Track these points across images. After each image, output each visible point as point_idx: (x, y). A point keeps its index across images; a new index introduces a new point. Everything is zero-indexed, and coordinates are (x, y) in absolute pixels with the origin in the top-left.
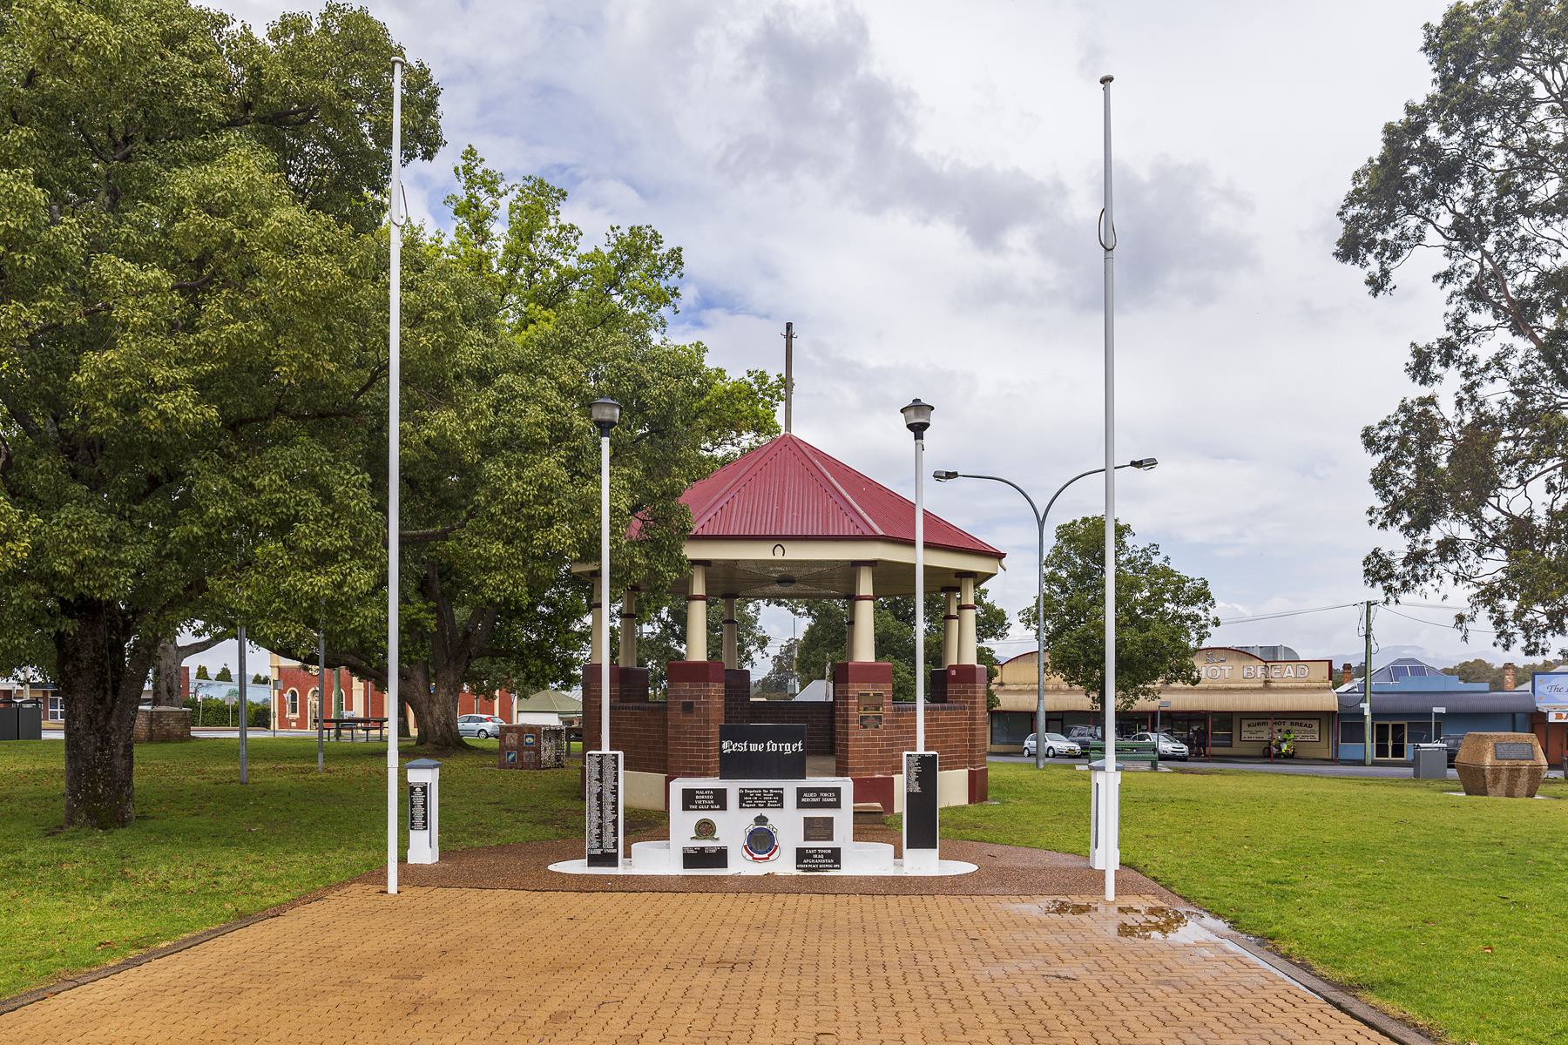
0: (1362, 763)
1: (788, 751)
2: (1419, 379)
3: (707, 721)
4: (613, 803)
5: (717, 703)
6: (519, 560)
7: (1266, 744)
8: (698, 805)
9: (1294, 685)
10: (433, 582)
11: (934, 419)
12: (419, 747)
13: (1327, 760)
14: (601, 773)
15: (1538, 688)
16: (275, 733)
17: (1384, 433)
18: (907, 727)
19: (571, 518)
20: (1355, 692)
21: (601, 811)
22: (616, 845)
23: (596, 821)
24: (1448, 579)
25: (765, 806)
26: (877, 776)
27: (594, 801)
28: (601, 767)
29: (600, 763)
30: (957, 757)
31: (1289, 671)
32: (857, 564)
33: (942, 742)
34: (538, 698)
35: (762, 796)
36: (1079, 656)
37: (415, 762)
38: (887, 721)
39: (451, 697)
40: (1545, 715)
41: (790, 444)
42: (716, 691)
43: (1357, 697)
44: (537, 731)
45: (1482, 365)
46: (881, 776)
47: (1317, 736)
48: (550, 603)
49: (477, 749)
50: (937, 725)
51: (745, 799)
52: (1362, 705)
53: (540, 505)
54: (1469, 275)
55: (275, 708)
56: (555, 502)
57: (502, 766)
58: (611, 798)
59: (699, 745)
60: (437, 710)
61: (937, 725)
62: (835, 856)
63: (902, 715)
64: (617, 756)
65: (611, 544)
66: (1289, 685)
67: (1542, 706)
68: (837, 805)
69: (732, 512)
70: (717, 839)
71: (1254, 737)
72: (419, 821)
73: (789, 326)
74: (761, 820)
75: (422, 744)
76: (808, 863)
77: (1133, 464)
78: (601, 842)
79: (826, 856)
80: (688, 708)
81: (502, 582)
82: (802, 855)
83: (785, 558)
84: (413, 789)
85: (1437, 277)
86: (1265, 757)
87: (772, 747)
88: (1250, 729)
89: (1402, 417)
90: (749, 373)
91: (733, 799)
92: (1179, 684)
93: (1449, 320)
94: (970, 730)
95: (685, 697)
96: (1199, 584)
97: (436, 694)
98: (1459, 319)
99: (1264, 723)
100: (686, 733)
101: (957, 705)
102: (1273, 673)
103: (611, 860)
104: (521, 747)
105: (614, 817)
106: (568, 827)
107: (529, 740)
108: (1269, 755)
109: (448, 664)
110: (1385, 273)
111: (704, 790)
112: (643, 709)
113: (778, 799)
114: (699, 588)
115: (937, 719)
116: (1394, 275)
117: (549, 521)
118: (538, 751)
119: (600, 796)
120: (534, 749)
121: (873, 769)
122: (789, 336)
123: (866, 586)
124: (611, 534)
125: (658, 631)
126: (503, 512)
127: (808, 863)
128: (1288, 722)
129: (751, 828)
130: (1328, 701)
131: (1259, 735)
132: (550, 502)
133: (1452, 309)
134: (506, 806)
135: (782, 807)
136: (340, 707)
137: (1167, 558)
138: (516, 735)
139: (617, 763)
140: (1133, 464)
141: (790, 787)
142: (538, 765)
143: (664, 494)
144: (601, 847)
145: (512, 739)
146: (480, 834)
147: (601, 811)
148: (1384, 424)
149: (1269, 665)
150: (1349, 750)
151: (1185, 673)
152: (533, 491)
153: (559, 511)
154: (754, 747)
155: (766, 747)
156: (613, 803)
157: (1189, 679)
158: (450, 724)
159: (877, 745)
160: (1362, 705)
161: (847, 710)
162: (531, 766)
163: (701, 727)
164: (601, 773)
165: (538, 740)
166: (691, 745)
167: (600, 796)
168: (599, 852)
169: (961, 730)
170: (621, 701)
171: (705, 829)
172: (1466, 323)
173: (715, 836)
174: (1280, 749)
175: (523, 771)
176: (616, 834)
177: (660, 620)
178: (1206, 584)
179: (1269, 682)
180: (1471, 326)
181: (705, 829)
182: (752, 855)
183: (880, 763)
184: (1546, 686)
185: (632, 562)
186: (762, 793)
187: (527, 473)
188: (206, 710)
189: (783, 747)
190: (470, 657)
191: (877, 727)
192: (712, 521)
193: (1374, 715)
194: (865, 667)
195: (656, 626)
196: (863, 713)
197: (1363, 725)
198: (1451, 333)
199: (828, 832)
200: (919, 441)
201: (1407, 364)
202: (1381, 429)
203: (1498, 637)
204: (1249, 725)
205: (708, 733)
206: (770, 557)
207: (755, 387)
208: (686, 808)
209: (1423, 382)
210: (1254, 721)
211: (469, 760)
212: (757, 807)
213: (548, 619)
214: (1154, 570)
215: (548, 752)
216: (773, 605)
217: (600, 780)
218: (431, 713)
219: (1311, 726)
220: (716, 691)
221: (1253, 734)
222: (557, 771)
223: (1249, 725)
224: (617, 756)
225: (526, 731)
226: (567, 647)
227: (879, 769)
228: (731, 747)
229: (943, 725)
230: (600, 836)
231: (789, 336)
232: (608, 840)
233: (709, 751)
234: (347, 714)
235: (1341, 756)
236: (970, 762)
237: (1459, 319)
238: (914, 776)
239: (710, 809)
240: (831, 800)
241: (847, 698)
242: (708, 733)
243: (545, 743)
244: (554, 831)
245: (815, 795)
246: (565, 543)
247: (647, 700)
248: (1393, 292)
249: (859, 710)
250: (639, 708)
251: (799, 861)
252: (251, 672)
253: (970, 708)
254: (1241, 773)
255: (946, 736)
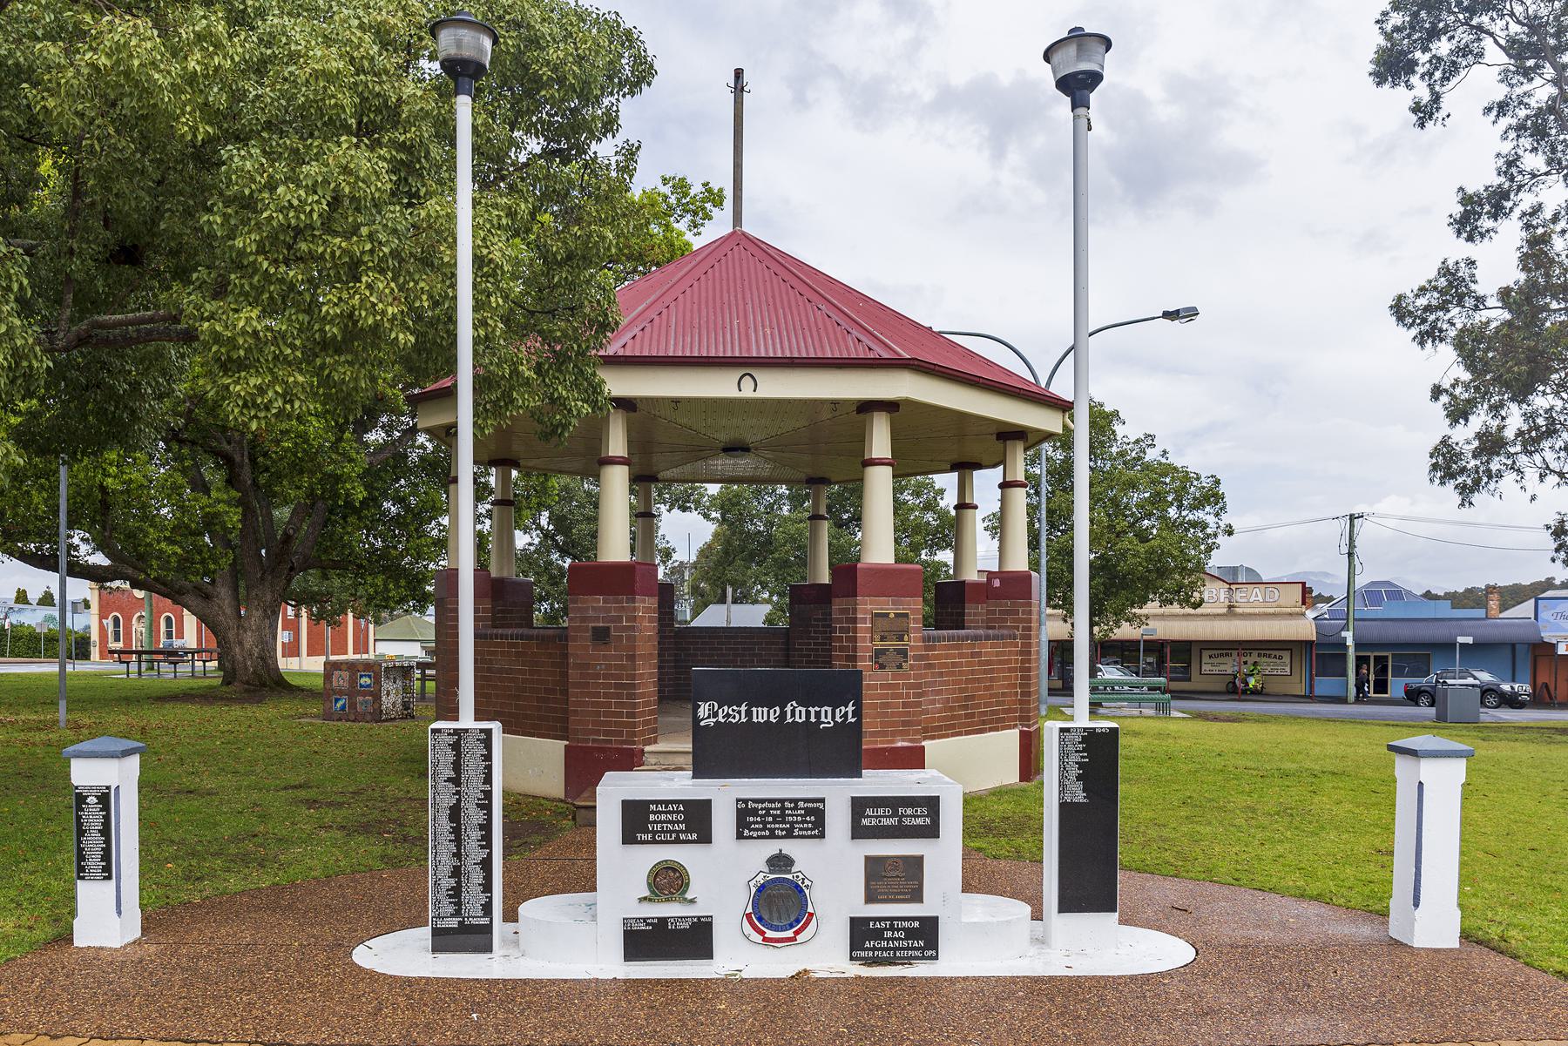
0: (1343, 700)
1: (827, 722)
2: (1465, 235)
3: (632, 658)
4: (481, 827)
5: (646, 628)
6: (293, 347)
7: (1230, 679)
8: (654, 833)
9: (1262, 610)
10: (242, 467)
11: (1112, 67)
12: (224, 689)
13: (1301, 696)
14: (457, 766)
15: (1543, 615)
16: (96, 664)
17: (1422, 302)
18: (825, 657)
19: (396, 265)
20: (1326, 619)
21: (458, 841)
22: (487, 909)
23: (447, 862)
24: (1531, 475)
25: (789, 835)
26: (899, 744)
27: (445, 824)
28: (458, 755)
29: (456, 747)
30: (1004, 711)
31: (1257, 594)
32: (868, 407)
33: (987, 688)
34: (390, 628)
35: (783, 815)
36: (1062, 570)
37: (86, 746)
38: (915, 658)
39: (267, 621)
40: (1553, 647)
41: (744, 242)
42: (646, 607)
43: (1338, 625)
44: (376, 668)
45: (1548, 214)
46: (906, 744)
47: (1288, 669)
48: (400, 500)
49: (303, 690)
50: (980, 663)
51: (749, 820)
52: (1344, 634)
53: (335, 234)
54: (1527, 106)
55: (95, 636)
56: (364, 231)
57: (328, 716)
58: (477, 817)
59: (619, 696)
60: (249, 639)
61: (980, 663)
62: (926, 934)
63: (933, 648)
64: (488, 732)
65: (475, 328)
66: (1257, 611)
67: (1548, 636)
68: (932, 831)
69: (668, 326)
70: (692, 901)
71: (1216, 670)
72: (94, 861)
73: (739, 74)
74: (780, 862)
75: (229, 683)
76: (874, 949)
77: (1167, 315)
78: (459, 904)
79: (911, 934)
80: (601, 635)
81: (261, 390)
82: (862, 934)
83: (759, 394)
84: (81, 799)
85: (1488, 110)
86: (1228, 692)
87: (797, 713)
88: (1212, 660)
89: (1443, 282)
90: (665, 181)
91: (723, 821)
92: (1175, 608)
93: (1501, 162)
94: (1022, 669)
95: (597, 619)
96: (1206, 483)
97: (248, 617)
98: (1512, 162)
99: (1227, 655)
100: (597, 676)
101: (1005, 632)
102: (1238, 596)
103: (474, 938)
104: (353, 691)
105: (483, 854)
106: (405, 839)
107: (365, 681)
108: (1234, 690)
109: (262, 579)
110: (1436, 98)
111: (667, 803)
112: (530, 638)
113: (813, 819)
114: (617, 445)
115: (979, 654)
116: (1446, 103)
117: (353, 269)
118: (377, 697)
119: (455, 813)
120: (371, 694)
121: (894, 734)
122: (739, 87)
123: (880, 443)
124: (476, 309)
125: (537, 541)
126: (261, 250)
127: (874, 949)
128: (1255, 653)
129: (760, 879)
130: (1304, 628)
131: (1222, 667)
132: (355, 230)
133: (1507, 147)
134: (311, 794)
135: (822, 836)
136: (169, 635)
137: (1165, 452)
138: (346, 675)
139: (488, 746)
140: (1167, 315)
141: (836, 793)
142: (377, 716)
143: (570, 257)
144: (458, 913)
145: (341, 680)
146: (245, 859)
147: (458, 841)
148: (1423, 290)
149: (1233, 587)
150: (1325, 685)
151: (1184, 595)
152: (318, 206)
153: (372, 251)
154: (761, 715)
155: (783, 715)
156: (481, 827)
157: (1187, 601)
158: (267, 658)
159: (899, 696)
160: (1344, 634)
161: (855, 639)
162: (369, 717)
163: (622, 667)
164: (457, 766)
165: (377, 681)
166: (606, 695)
167: (455, 813)
168: (453, 923)
169: (1010, 670)
170: (494, 627)
171: (668, 881)
172: (1521, 166)
173: (689, 896)
174: (1247, 684)
175: (357, 724)
176: (487, 887)
177: (539, 527)
178: (1218, 482)
179: (1233, 606)
180: (1528, 169)
181: (668, 881)
182: (762, 933)
183: (904, 723)
184: (1552, 612)
185: (515, 372)
186: (783, 809)
187: (312, 169)
188: (16, 638)
189: (818, 714)
190: (292, 569)
191: (900, 667)
192: (648, 330)
193: (1358, 646)
194: (881, 572)
195: (534, 534)
196: (879, 645)
197: (1344, 657)
198: (1502, 179)
199: (913, 884)
200: (1081, 111)
201: (1451, 216)
202: (1417, 296)
203: (1557, 550)
204: (1210, 657)
205: (633, 677)
206: (734, 393)
207: (673, 200)
208: (629, 838)
209: (1470, 239)
210: (1219, 652)
211: (287, 707)
212: (773, 836)
213: (397, 521)
214: (1147, 467)
215: (391, 696)
216: (675, 511)
217: (456, 781)
218: (241, 643)
219: (1281, 658)
220: (647, 610)
221: (1213, 668)
222: (402, 724)
223: (1210, 657)
224: (488, 732)
225: (361, 668)
226: (419, 556)
227: (902, 733)
228: (715, 715)
229: (988, 663)
230: (456, 893)
231: (739, 87)
232: (473, 899)
233: (635, 705)
234: (177, 643)
235: (1318, 691)
236: (1021, 718)
237: (1512, 162)
238: (1074, 771)
239: (678, 841)
240: (919, 821)
241: (855, 620)
242: (633, 677)
243: (387, 685)
244: (377, 850)
245: (888, 810)
246: (384, 313)
247: (530, 625)
248: (1447, 121)
249: (872, 640)
250: (522, 637)
251: (856, 942)
252: (70, 597)
253: (1023, 637)
254: (1296, 718)
255: (992, 680)
